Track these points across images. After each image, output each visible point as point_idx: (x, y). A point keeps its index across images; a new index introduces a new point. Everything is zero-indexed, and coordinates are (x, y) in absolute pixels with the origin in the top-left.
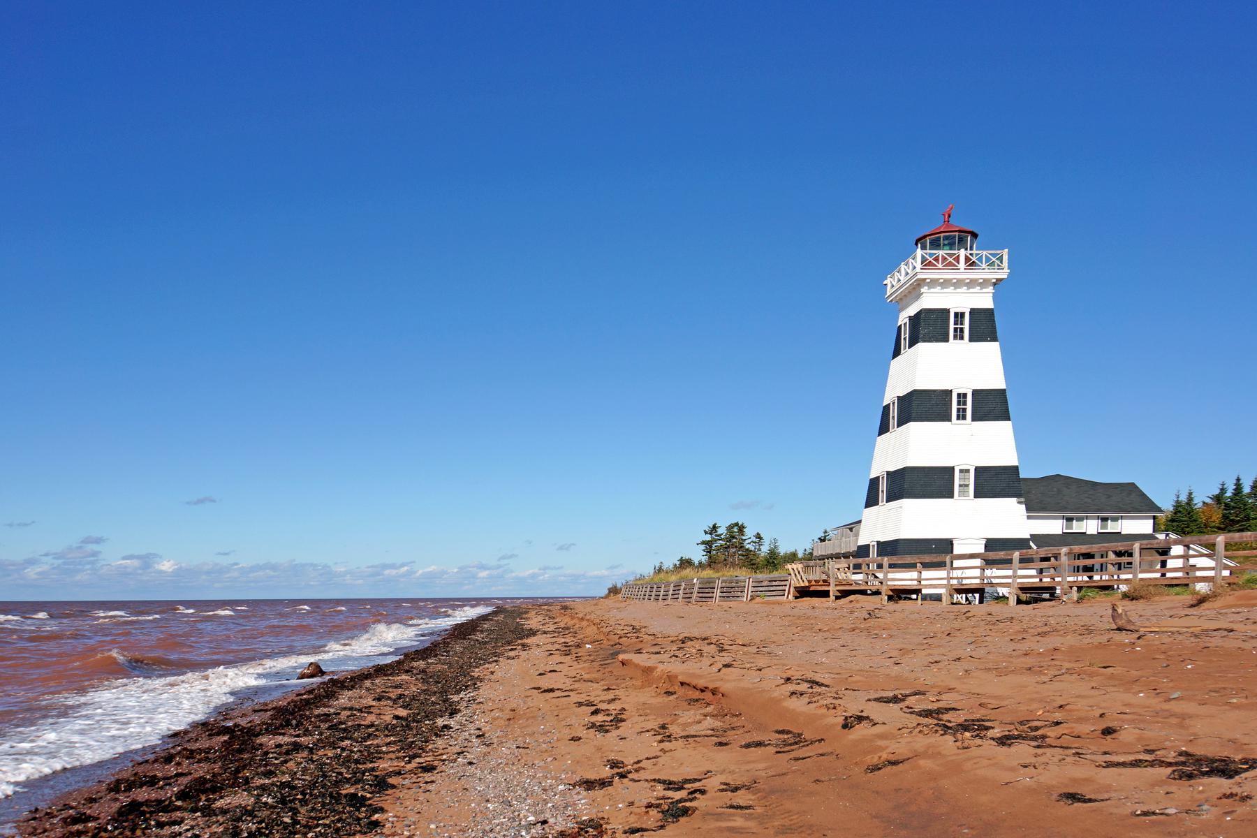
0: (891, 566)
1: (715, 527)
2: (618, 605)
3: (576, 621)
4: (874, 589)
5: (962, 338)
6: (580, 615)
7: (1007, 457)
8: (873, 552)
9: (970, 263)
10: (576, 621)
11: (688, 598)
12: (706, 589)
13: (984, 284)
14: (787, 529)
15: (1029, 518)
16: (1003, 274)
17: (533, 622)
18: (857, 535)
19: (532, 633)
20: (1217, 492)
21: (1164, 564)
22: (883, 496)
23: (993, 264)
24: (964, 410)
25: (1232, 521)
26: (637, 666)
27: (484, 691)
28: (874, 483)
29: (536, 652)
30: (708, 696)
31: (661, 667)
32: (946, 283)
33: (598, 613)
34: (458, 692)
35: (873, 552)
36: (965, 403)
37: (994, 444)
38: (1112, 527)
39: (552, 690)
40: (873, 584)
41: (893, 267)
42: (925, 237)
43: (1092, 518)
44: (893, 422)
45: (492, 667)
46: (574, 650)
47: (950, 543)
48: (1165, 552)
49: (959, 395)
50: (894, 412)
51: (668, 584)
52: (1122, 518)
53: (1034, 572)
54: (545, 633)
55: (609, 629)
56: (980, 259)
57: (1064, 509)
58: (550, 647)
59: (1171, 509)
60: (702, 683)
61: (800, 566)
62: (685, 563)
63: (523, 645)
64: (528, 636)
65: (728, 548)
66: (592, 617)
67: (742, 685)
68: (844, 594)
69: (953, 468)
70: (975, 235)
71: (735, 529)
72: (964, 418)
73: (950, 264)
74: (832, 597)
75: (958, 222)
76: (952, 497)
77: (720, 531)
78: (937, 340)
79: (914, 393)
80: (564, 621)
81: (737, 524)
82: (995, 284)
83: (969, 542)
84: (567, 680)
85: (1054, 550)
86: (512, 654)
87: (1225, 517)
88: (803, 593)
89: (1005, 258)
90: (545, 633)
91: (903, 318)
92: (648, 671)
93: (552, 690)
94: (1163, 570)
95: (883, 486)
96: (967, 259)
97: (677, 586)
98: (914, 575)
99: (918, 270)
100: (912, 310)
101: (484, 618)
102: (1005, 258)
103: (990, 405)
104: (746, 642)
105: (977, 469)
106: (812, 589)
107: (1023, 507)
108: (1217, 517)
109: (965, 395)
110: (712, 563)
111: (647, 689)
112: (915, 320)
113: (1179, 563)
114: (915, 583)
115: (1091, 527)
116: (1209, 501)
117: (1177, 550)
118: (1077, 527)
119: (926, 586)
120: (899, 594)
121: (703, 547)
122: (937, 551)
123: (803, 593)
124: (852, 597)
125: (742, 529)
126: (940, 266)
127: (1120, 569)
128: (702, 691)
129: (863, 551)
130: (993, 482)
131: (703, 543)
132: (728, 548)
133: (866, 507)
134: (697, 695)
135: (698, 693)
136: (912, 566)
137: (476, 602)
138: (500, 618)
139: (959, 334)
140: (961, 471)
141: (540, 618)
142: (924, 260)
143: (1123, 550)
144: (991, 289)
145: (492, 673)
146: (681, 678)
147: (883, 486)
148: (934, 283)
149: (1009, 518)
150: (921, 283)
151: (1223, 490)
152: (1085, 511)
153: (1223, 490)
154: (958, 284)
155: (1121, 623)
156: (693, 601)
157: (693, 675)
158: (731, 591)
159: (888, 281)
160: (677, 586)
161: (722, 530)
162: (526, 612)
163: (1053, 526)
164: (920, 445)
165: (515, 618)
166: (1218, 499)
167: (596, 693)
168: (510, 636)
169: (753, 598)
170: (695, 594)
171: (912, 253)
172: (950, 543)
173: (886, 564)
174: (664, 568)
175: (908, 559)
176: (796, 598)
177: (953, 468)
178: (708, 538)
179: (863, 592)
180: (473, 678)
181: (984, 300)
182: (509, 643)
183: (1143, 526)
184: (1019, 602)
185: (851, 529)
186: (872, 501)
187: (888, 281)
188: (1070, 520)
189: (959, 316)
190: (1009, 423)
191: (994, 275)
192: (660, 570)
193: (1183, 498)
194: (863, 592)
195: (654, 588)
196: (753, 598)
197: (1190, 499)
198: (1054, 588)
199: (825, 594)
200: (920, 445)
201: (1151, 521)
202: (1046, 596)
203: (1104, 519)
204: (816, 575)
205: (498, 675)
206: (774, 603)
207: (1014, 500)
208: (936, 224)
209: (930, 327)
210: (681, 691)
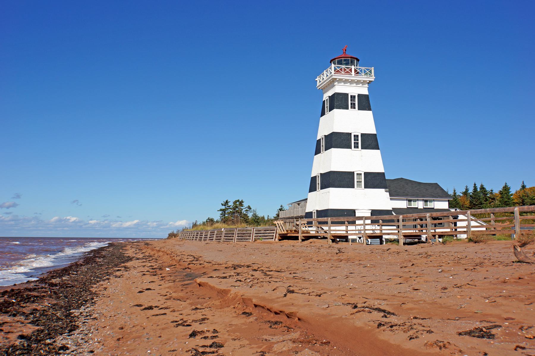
0: (333, 223)
1: (227, 202)
2: (178, 243)
3: (155, 252)
4: (322, 235)
5: (354, 108)
6: (158, 249)
8: (315, 216)
9: (357, 73)
10: (155, 252)
11: (218, 239)
12: (229, 236)
13: (364, 83)
14: (264, 204)
15: (391, 199)
16: (372, 79)
17: (130, 252)
18: (305, 206)
19: (130, 259)
20: (464, 190)
21: (455, 224)
22: (318, 186)
23: (367, 74)
24: (358, 143)
25: (474, 204)
26: (212, 288)
27: (100, 307)
28: (314, 179)
29: (134, 272)
30: (282, 318)
31: (233, 291)
32: (346, 81)
33: (168, 247)
34: (79, 307)
35: (315, 216)
36: (358, 140)
37: (371, 161)
38: (430, 205)
39: (151, 308)
40: (321, 233)
41: (320, 73)
42: (335, 59)
43: (420, 200)
44: (323, 148)
45: (105, 284)
46: (159, 272)
47: (354, 211)
48: (456, 217)
49: (355, 136)
50: (323, 143)
51: (207, 232)
52: (434, 200)
53: (395, 228)
54: (138, 259)
55: (178, 258)
56: (361, 71)
57: (407, 195)
58: (142, 269)
60: (276, 307)
61: (282, 222)
62: (211, 221)
63: (125, 267)
64: (127, 261)
65: (234, 213)
66: (165, 249)
68: (307, 238)
70: (358, 60)
71: (238, 203)
73: (347, 72)
74: (300, 240)
75: (349, 54)
76: (354, 187)
77: (229, 204)
79: (333, 134)
80: (148, 252)
81: (238, 201)
82: (368, 83)
83: (363, 211)
84: (160, 298)
85: (422, 215)
86: (118, 273)
88: (284, 237)
89: (373, 71)
90: (138, 259)
91: (326, 96)
92: (223, 293)
93: (151, 308)
94: (455, 227)
95: (319, 181)
96: (355, 71)
97: (212, 233)
98: (343, 228)
99: (333, 74)
100: (330, 93)
101: (102, 249)
102: (373, 71)
103: (369, 142)
104: (279, 269)
105: (365, 173)
106: (289, 235)
107: (388, 193)
108: (467, 203)
110: (225, 221)
111: (226, 309)
112: (332, 98)
113: (465, 224)
114: (344, 232)
115: (420, 205)
117: (461, 217)
118: (414, 205)
119: (352, 234)
120: (336, 239)
121: (221, 212)
122: (348, 216)
123: (284, 237)
124: (311, 240)
125: (241, 203)
126: (343, 73)
127: (435, 226)
128: (276, 313)
129: (309, 215)
130: (373, 180)
131: (221, 210)
132: (234, 213)
134: (272, 317)
135: (272, 315)
136: (342, 223)
137: (99, 240)
138: (111, 249)
139: (353, 106)
140: (357, 174)
141: (133, 250)
142: (335, 70)
143: (438, 218)
144: (367, 85)
145: (105, 289)
146: (255, 301)
147: (319, 181)
148: (340, 81)
149: (381, 199)
150: (334, 80)
151: (467, 190)
152: (417, 196)
153: (467, 190)
154: (352, 82)
155: (521, 258)
156: (221, 241)
157: (264, 299)
158: (243, 236)
159: (317, 79)
160: (212, 233)
161: (231, 204)
162: (125, 246)
163: (402, 204)
164: (337, 160)
165: (119, 250)
166: (465, 193)
167: (185, 310)
168: (116, 261)
169: (255, 240)
170: (223, 237)
171: (329, 66)
172: (354, 211)
173: (329, 222)
174: (198, 223)
175: (342, 219)
176: (280, 240)
178: (223, 207)
179: (316, 237)
180: (91, 293)
181: (364, 90)
182: (116, 266)
183: (444, 205)
184: (404, 244)
185: (299, 204)
186: (313, 188)
187: (317, 79)
188: (410, 201)
189: (353, 97)
190: (378, 152)
191: (368, 80)
192: (195, 225)
194: (316, 237)
195: (199, 232)
196: (255, 240)
198: (420, 236)
199: (296, 238)
200: (337, 160)
201: (447, 203)
202: (344, 240)
204: (288, 227)
205: (110, 290)
206: (267, 243)
207: (383, 190)
208: (340, 54)
209: (339, 101)
210: (256, 312)
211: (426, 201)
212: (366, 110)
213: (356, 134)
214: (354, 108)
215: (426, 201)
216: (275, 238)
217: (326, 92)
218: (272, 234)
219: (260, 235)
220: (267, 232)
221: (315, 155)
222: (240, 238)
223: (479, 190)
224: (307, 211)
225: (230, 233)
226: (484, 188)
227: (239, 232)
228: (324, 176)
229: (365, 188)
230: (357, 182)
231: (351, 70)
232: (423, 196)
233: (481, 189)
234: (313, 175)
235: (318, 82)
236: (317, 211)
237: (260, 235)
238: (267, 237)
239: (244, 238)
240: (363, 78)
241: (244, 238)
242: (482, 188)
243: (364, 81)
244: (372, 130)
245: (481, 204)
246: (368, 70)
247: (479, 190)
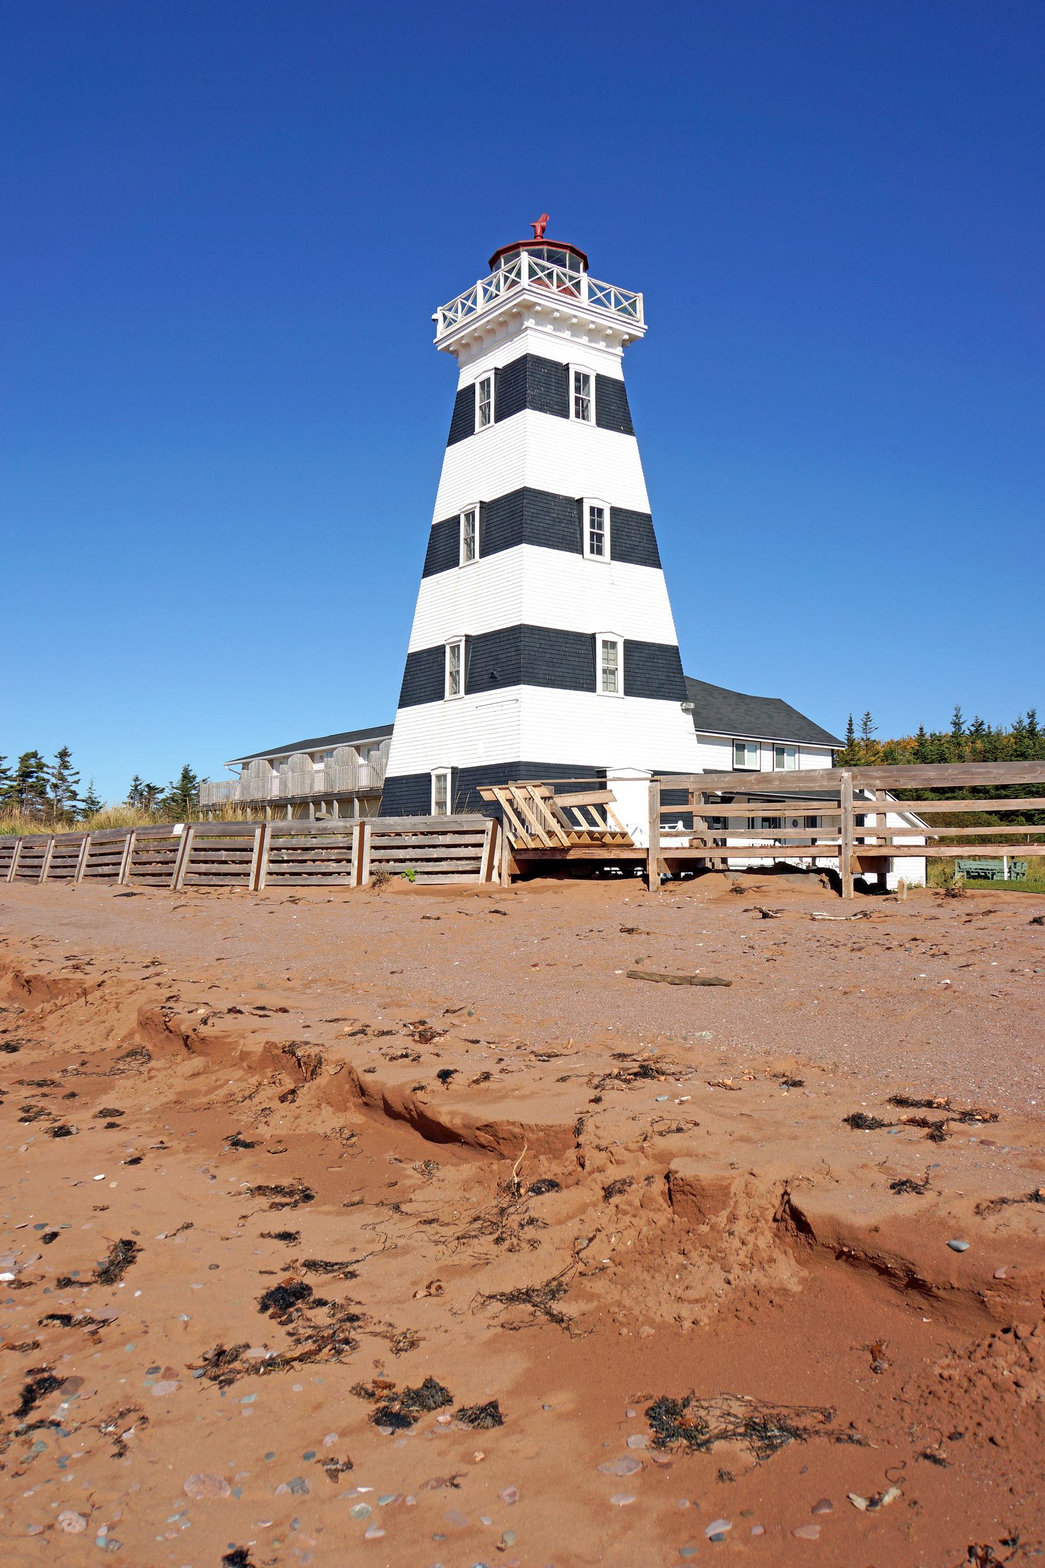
7: (662, 631)
16: (638, 327)
32: (561, 322)
35: (441, 794)
37: (621, 602)
52: (799, 750)
67: (297, 1132)
73: (567, 291)
89: (640, 306)
100: (504, 356)
103: (634, 539)
105: (628, 643)
107: (691, 717)
112: (504, 375)
123: (534, 866)
130: (652, 671)
133: (401, 706)
140: (605, 643)
144: (619, 351)
148: (545, 316)
152: (762, 734)
154: (578, 329)
159: (438, 316)
169: (379, 879)
176: (514, 878)
187: (438, 316)
188: (740, 747)
207: (677, 705)
209: (531, 386)
212: (619, 430)
213: (598, 504)
215: (780, 751)
216: (490, 867)
217: (472, 359)
218: (471, 852)
219: (401, 854)
220: (442, 840)
221: (425, 576)
222: (285, 867)
224: (392, 772)
225: (226, 842)
227: (281, 842)
228: (481, 647)
229: (626, 693)
230: (605, 671)
232: (775, 735)
234: (419, 643)
235: (441, 326)
236: (454, 770)
237: (401, 854)
238: (444, 866)
239: (309, 867)
240: (610, 319)
241: (309, 867)
243: (616, 334)
244: (639, 502)
246: (627, 298)
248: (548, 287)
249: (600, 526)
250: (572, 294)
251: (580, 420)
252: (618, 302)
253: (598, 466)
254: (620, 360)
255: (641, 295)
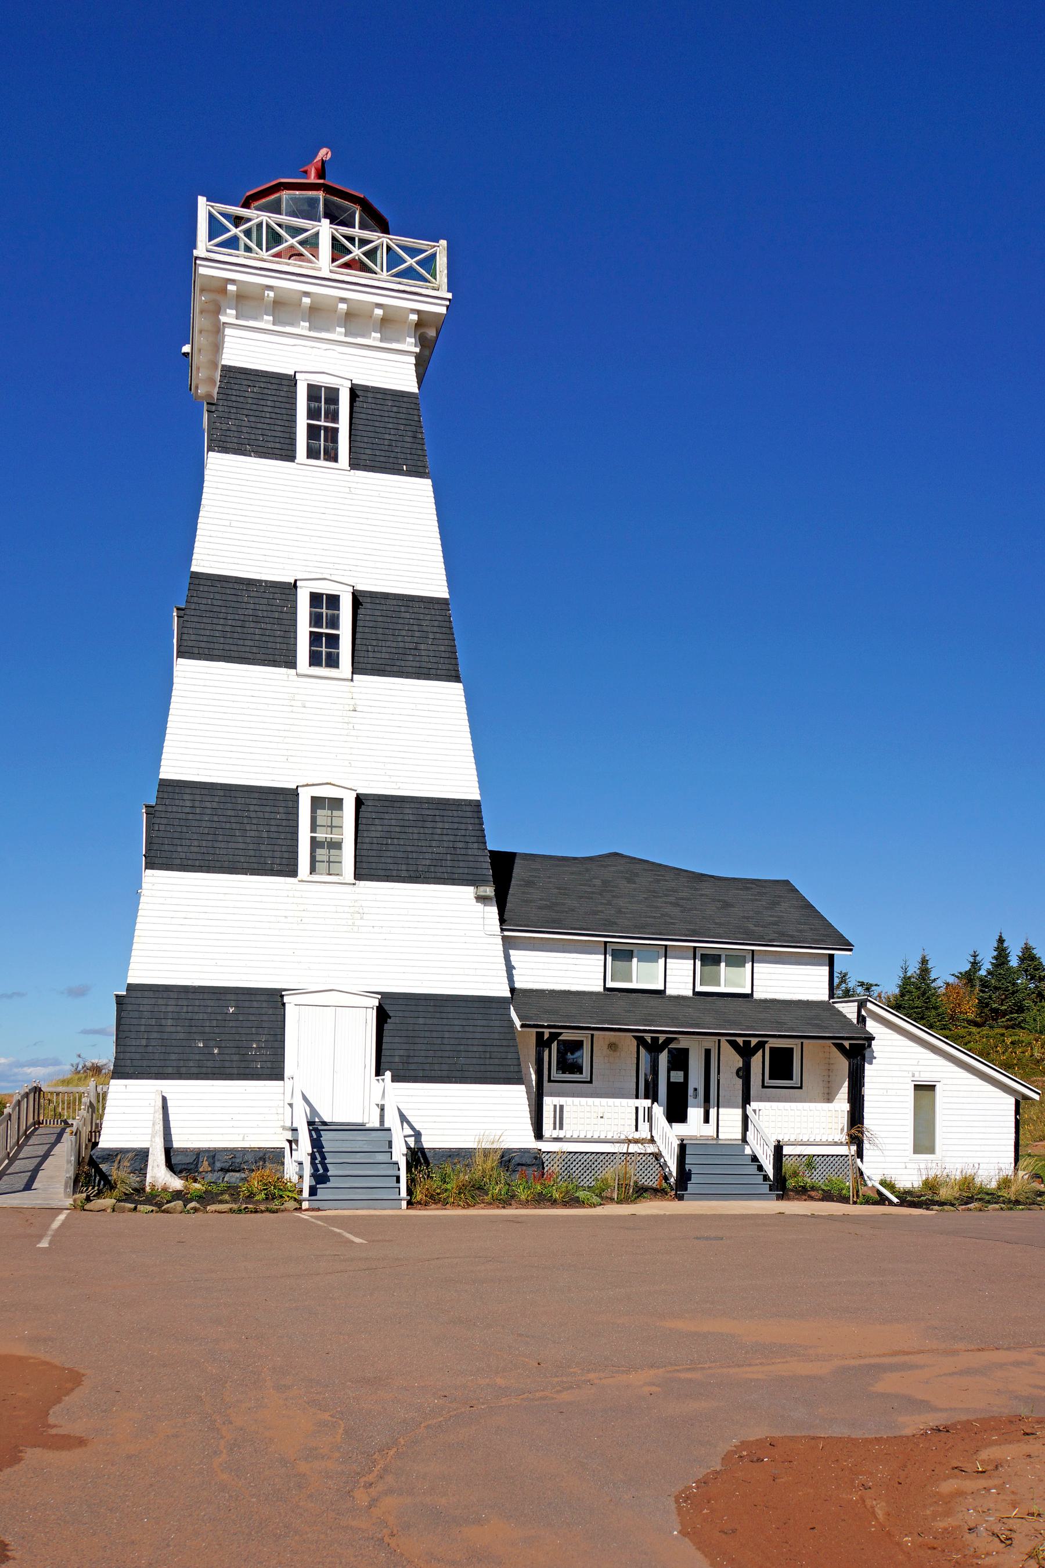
7: (456, 778)
13: (388, 323)
20: (967, 967)
25: (995, 1011)
32: (283, 308)
37: (419, 738)
38: (731, 980)
49: (316, 599)
52: (753, 957)
57: (608, 925)
59: (897, 991)
69: (292, 795)
72: (333, 662)
78: (366, 389)
87: (983, 1004)
89: (442, 262)
103: (393, 637)
105: (360, 801)
107: (493, 910)
108: (970, 1009)
109: (334, 601)
115: (679, 977)
116: (951, 980)
118: (644, 975)
130: (403, 840)
140: (317, 802)
148: (248, 301)
149: (449, 941)
151: (975, 965)
152: (660, 933)
153: (975, 965)
154: (318, 315)
163: (573, 971)
166: (969, 977)
177: (292, 795)
181: (395, 371)
193: (913, 970)
197: (924, 971)
203: (711, 960)
207: (469, 891)
211: (711, 960)
213: (325, 588)
214: (332, 456)
223: (1014, 962)
226: (1033, 958)
229: (358, 876)
231: (312, 243)
232: (694, 934)
233: (1022, 959)
240: (379, 291)
242: (1028, 956)
244: (429, 579)
245: (1021, 1009)
247: (1014, 962)
248: (426, 280)
249: (334, 623)
250: (364, 268)
251: (321, 462)
252: (394, 259)
253: (382, 533)
254: (413, 360)
255: (443, 243)
